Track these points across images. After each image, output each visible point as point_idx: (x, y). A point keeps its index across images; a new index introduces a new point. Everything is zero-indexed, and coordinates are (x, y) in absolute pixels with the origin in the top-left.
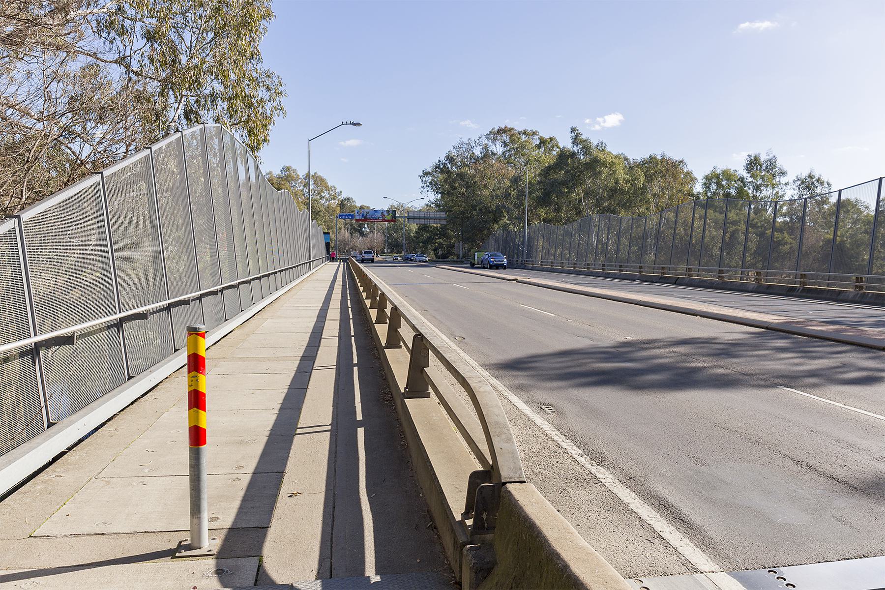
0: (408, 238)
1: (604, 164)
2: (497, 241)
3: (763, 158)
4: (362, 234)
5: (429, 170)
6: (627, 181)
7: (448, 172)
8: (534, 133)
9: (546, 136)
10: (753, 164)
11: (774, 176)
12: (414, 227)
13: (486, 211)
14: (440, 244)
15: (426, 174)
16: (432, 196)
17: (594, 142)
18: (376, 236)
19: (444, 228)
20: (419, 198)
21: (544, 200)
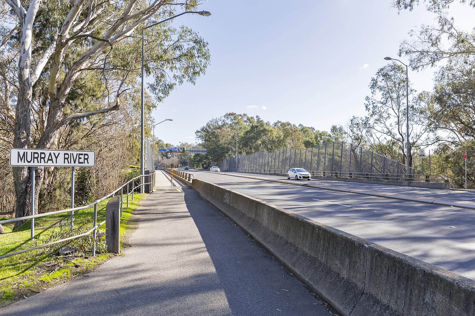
0: (190, 159)
1: (268, 131)
2: (227, 161)
3: (338, 127)
4: (167, 157)
5: (200, 130)
6: (277, 138)
7: (208, 132)
8: (245, 115)
9: (250, 116)
10: (334, 129)
11: (342, 134)
12: (193, 154)
13: (223, 148)
14: (205, 162)
15: (198, 132)
16: (200, 141)
17: (265, 121)
18: (175, 159)
19: (206, 155)
20: (194, 141)
21: (245, 145)
